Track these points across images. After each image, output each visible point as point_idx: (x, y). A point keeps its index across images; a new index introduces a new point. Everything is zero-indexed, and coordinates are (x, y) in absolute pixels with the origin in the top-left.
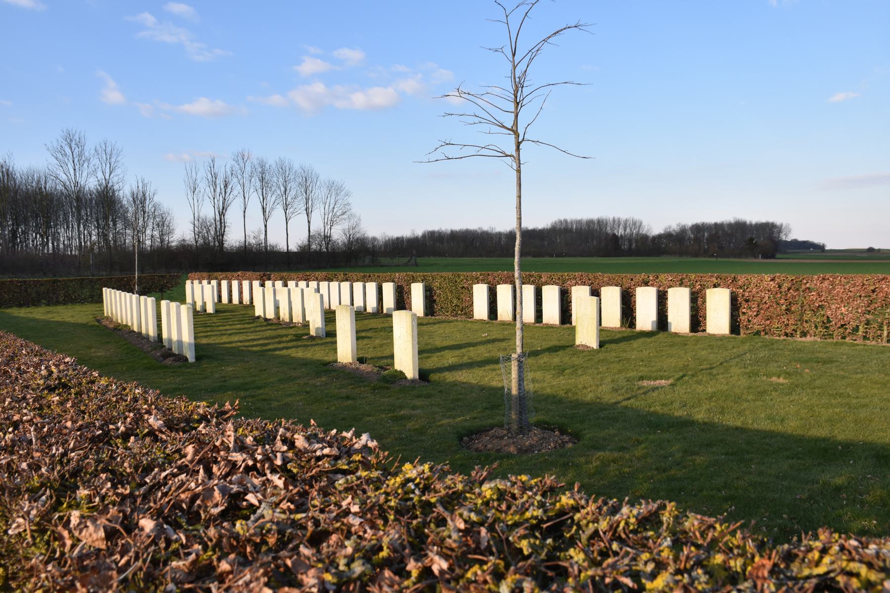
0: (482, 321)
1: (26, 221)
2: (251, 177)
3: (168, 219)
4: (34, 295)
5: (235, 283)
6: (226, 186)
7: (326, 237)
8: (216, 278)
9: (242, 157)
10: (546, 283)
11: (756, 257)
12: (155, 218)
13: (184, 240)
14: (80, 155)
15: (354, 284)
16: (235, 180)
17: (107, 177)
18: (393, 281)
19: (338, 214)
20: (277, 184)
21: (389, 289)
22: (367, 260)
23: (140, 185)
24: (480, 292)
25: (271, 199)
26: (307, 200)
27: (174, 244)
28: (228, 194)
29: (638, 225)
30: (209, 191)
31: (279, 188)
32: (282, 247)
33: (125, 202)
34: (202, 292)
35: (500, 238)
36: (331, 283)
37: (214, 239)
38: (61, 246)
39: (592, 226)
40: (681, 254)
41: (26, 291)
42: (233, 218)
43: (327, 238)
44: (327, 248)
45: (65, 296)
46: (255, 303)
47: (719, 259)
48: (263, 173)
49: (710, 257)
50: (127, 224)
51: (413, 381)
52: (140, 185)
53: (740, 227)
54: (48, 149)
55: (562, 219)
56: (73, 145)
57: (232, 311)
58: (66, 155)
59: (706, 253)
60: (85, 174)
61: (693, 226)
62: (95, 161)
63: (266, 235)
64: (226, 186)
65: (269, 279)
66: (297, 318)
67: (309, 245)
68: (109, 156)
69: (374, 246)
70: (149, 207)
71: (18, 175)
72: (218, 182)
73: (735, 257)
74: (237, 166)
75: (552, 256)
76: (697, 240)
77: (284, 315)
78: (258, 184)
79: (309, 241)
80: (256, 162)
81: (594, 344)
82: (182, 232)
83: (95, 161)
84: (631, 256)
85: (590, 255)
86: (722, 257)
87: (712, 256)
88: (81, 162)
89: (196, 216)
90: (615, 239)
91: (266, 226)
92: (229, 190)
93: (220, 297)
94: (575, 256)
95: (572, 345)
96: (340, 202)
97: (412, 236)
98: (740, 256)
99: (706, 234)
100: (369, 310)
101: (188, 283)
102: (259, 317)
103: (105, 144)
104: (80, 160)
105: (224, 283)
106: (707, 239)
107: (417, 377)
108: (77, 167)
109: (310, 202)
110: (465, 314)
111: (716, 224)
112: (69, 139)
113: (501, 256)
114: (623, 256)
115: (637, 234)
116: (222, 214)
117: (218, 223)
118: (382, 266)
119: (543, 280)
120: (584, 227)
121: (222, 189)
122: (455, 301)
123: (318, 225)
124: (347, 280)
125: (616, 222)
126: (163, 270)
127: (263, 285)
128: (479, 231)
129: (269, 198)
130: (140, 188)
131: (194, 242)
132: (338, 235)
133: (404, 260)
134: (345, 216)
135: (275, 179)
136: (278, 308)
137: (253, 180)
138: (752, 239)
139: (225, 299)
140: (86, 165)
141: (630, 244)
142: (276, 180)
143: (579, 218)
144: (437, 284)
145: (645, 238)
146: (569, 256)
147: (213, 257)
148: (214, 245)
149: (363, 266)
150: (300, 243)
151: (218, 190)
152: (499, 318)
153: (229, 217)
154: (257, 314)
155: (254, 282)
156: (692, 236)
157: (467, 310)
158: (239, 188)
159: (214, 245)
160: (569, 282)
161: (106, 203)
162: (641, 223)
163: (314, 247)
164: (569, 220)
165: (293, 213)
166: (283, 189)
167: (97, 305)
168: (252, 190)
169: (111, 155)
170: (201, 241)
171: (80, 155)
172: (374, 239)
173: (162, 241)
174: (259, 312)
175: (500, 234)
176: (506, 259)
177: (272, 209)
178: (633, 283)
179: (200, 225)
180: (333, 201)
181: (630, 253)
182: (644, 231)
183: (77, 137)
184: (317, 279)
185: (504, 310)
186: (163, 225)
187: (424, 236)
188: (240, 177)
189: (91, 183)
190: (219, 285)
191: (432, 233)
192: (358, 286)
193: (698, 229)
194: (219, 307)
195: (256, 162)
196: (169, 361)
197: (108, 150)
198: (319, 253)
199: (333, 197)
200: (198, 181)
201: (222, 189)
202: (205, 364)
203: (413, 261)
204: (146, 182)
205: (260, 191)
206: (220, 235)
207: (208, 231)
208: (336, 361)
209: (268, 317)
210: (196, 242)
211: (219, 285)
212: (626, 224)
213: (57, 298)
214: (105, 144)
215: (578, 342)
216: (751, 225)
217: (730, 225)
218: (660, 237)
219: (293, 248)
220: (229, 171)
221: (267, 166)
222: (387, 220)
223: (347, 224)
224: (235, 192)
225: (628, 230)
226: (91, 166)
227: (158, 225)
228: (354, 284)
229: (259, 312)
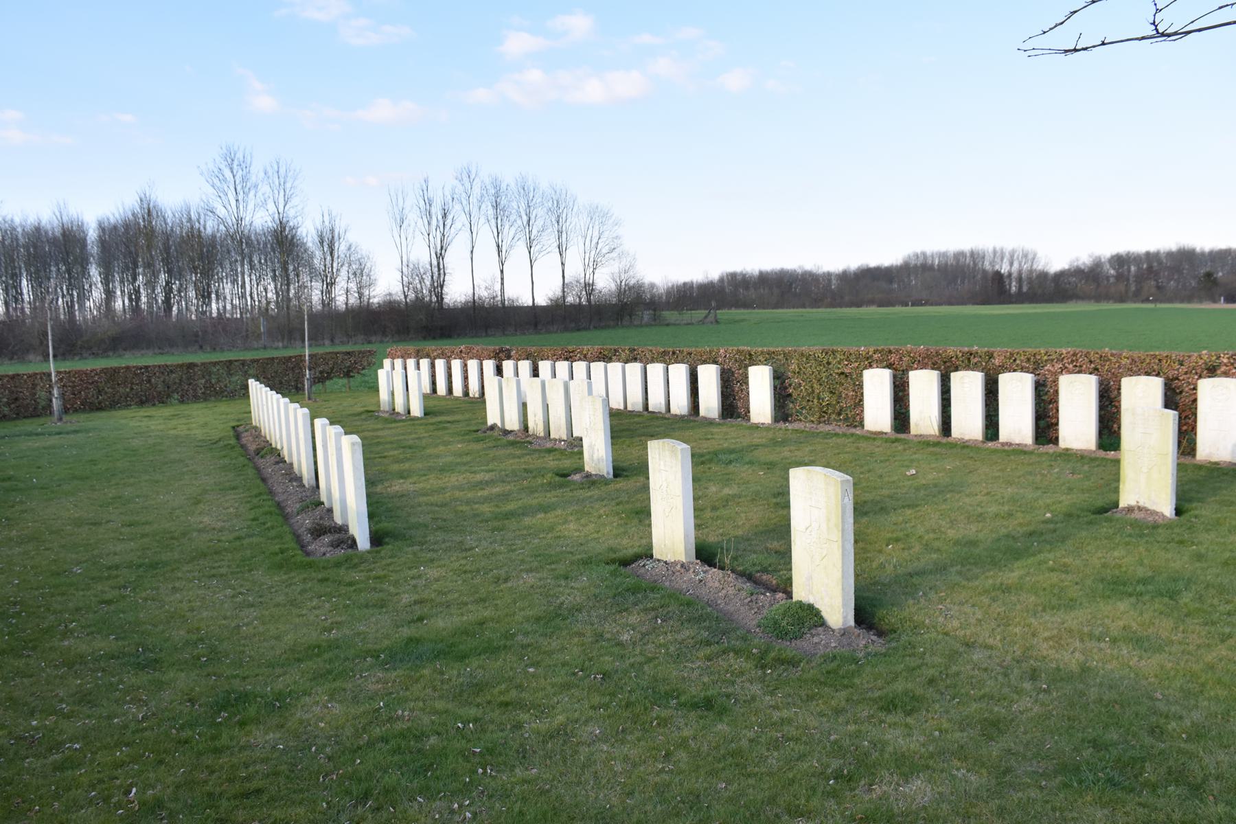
1: (180, 276)
2: (481, 201)
3: (368, 265)
4: (160, 387)
5: (456, 364)
6: (445, 216)
7: (586, 285)
8: (428, 356)
9: (467, 176)
10: (1004, 368)
11: (1215, 301)
12: (350, 265)
13: (390, 294)
14: (244, 180)
15: (649, 366)
16: (458, 207)
17: (281, 210)
18: (715, 362)
19: (604, 251)
21: (709, 376)
23: (327, 219)
25: (508, 233)
26: (560, 232)
27: (375, 300)
28: (447, 227)
29: (1030, 257)
30: (422, 224)
32: (526, 301)
33: (310, 244)
35: (830, 280)
36: (609, 365)
37: (430, 292)
38: (229, 307)
39: (962, 260)
40: (1098, 298)
41: (149, 381)
42: (455, 261)
43: (589, 287)
45: (206, 388)
47: (1160, 306)
50: (313, 273)
51: (844, 632)
52: (327, 219)
53: (1185, 258)
54: (202, 174)
55: (919, 251)
57: (450, 412)
58: (225, 180)
61: (1113, 257)
62: (264, 189)
63: (502, 284)
64: (445, 216)
65: (509, 357)
66: (558, 431)
67: (564, 297)
68: (283, 181)
69: (653, 296)
70: (341, 248)
71: (169, 213)
72: (433, 211)
73: (1182, 301)
74: (461, 188)
75: (907, 305)
76: (1119, 277)
77: (536, 423)
78: (491, 212)
80: (487, 181)
81: (1165, 505)
82: (387, 285)
83: (264, 189)
84: (1022, 302)
85: (962, 302)
86: (1161, 302)
87: (1147, 300)
90: (998, 277)
91: (502, 272)
92: (448, 222)
93: (434, 383)
94: (940, 304)
95: (1108, 508)
96: (606, 234)
97: (706, 281)
98: (1189, 299)
99: (1133, 268)
100: (675, 409)
102: (493, 427)
104: (242, 188)
105: (440, 364)
106: (1136, 276)
107: (852, 623)
108: (240, 198)
109: (564, 236)
111: (1148, 254)
112: (230, 159)
113: (832, 305)
114: (1011, 302)
115: (1031, 271)
116: (440, 256)
117: (435, 270)
118: (668, 325)
119: (997, 362)
120: (951, 261)
121: (440, 220)
122: (826, 396)
123: (575, 270)
124: (635, 360)
125: (998, 254)
127: (499, 371)
128: (800, 271)
130: (327, 223)
132: (605, 282)
133: (700, 314)
134: (614, 254)
135: (514, 204)
136: (524, 405)
137: (483, 207)
138: (1209, 275)
139: (442, 389)
140: (252, 193)
142: (516, 205)
143: (943, 249)
144: (794, 367)
145: (1043, 275)
146: (932, 305)
147: (429, 322)
149: (641, 326)
150: (551, 295)
151: (434, 222)
152: (914, 430)
153: (450, 260)
154: (490, 422)
155: (485, 362)
156: (1112, 272)
157: (853, 411)
158: (462, 220)
160: (1048, 367)
161: (283, 246)
162: (1035, 255)
163: (570, 299)
166: (525, 218)
167: (868, 497)
168: (483, 220)
169: (286, 176)
170: (412, 296)
171: (244, 180)
172: (652, 286)
173: (361, 295)
174: (493, 418)
176: (839, 310)
178: (1184, 369)
179: (410, 272)
180: (596, 234)
181: (1021, 298)
182: (1040, 266)
183: (240, 155)
184: (585, 358)
185: (924, 416)
187: (721, 280)
188: (465, 202)
189: (260, 219)
190: (433, 366)
191: (733, 276)
192: (656, 369)
193: (1120, 261)
194: (431, 403)
195: (487, 181)
196: (321, 546)
197: (282, 171)
198: (577, 308)
199: (597, 228)
201: (440, 220)
203: (712, 316)
205: (493, 222)
206: (438, 287)
207: (422, 280)
209: (508, 427)
210: (406, 297)
211: (433, 366)
212: (1012, 256)
215: (1127, 498)
216: (1203, 254)
217: (1170, 254)
218: (1060, 275)
219: (542, 301)
220: (448, 194)
221: (504, 186)
223: (616, 265)
224: (458, 225)
225: (1016, 265)
226: (260, 194)
227: (355, 274)
229: (493, 418)
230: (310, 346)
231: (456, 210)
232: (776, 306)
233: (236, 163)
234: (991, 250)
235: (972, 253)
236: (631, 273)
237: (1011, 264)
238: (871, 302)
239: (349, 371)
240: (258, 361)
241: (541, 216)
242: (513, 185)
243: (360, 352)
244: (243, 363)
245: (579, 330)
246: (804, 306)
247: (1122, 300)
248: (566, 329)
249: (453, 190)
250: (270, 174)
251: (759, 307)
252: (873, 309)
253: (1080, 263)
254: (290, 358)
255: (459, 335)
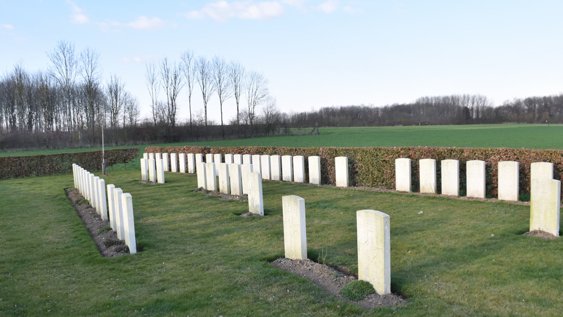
0: (403, 193)
2: (194, 70)
3: (135, 104)
4: (26, 168)
6: (176, 78)
7: (250, 114)
8: (167, 152)
9: (188, 57)
12: (126, 104)
13: (147, 119)
15: (283, 157)
16: (182, 73)
18: (317, 155)
19: (259, 96)
20: (210, 74)
21: (314, 162)
22: (282, 130)
24: (402, 167)
25: (209, 87)
26: (236, 87)
27: (139, 122)
28: (177, 84)
29: (483, 99)
30: (164, 82)
31: (215, 78)
33: (105, 93)
34: (154, 165)
35: (378, 112)
36: (262, 156)
37: (168, 118)
38: (62, 126)
39: (447, 101)
40: (518, 121)
41: (20, 165)
43: (251, 115)
44: (251, 122)
46: (198, 173)
47: (551, 125)
48: (203, 67)
49: (542, 123)
50: (107, 108)
51: (385, 297)
54: (48, 56)
56: (65, 52)
57: (178, 181)
58: (60, 59)
59: (540, 120)
60: (74, 73)
61: (526, 100)
62: (81, 63)
63: (206, 114)
64: (176, 78)
65: (209, 152)
66: (235, 191)
67: (238, 121)
68: (90, 59)
70: (121, 95)
71: (31, 76)
72: (170, 75)
75: (418, 125)
76: (530, 110)
78: (200, 76)
79: (238, 118)
82: (145, 114)
83: (81, 63)
84: (479, 123)
86: (552, 123)
87: (544, 122)
88: (71, 64)
89: (155, 101)
91: (206, 107)
92: (178, 81)
93: (170, 166)
94: (436, 124)
96: (260, 87)
97: (313, 112)
99: (537, 105)
101: (145, 155)
102: (201, 189)
103: (88, 50)
104: (69, 64)
106: (539, 110)
108: (68, 68)
109: (238, 88)
110: (386, 185)
111: (545, 98)
112: (63, 48)
114: (473, 123)
115: (483, 107)
116: (173, 99)
117: (171, 106)
118: (293, 135)
122: (376, 173)
123: (244, 106)
124: (275, 153)
126: (120, 147)
128: (362, 107)
129: (207, 86)
130: (114, 82)
131: (153, 121)
132: (260, 113)
133: (310, 129)
134: (264, 98)
137: (196, 73)
139: (174, 169)
140: (74, 66)
141: (478, 115)
142: (212, 72)
143: (547, 95)
145: (490, 109)
146: (431, 124)
147: (166, 134)
148: (168, 122)
149: (279, 136)
150: (231, 119)
151: (170, 81)
152: (422, 190)
153: (178, 101)
154: (199, 186)
155: (197, 155)
156: (526, 107)
158: (185, 80)
159: (168, 122)
160: (493, 157)
161: (90, 94)
162: (485, 98)
163: (241, 122)
164: (430, 97)
165: (225, 97)
166: (218, 79)
168: (195, 80)
170: (158, 120)
172: (285, 115)
174: (201, 184)
175: (377, 109)
177: (210, 94)
180: (255, 88)
181: (478, 121)
182: (488, 104)
183: (68, 46)
185: (427, 182)
186: (132, 108)
187: (321, 112)
188: (186, 71)
189: (78, 80)
190: (169, 157)
191: (327, 109)
192: (286, 159)
193: (530, 102)
194: (169, 176)
196: (110, 252)
198: (245, 126)
200: (155, 76)
202: (145, 253)
203: (316, 131)
204: (117, 77)
205: (201, 81)
206: (172, 115)
207: (164, 112)
208: (282, 256)
209: (209, 189)
210: (155, 120)
211: (169, 157)
212: (473, 99)
213: (44, 170)
214: (88, 50)
215: (534, 227)
218: (499, 109)
219: (226, 123)
221: (206, 62)
222: (294, 100)
224: (182, 83)
225: (475, 104)
226: (78, 67)
227: (128, 108)
228: (283, 157)
229: (201, 184)
230: (105, 146)
231: (181, 75)
232: (350, 125)
233: (66, 50)
234: (462, 96)
235: (453, 98)
236: (273, 108)
237: (473, 103)
238: (399, 123)
239: (125, 160)
240: (77, 154)
241: (226, 77)
242: (211, 62)
243: (131, 150)
244: (70, 155)
245: (246, 138)
246: (364, 126)
247: (531, 122)
248: (240, 138)
249: (180, 63)
250: (84, 56)
251: (340, 126)
252: (400, 127)
253: (509, 103)
254: (94, 152)
255: (183, 141)
